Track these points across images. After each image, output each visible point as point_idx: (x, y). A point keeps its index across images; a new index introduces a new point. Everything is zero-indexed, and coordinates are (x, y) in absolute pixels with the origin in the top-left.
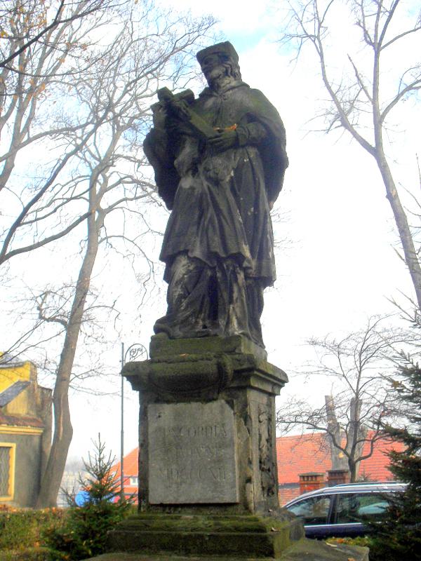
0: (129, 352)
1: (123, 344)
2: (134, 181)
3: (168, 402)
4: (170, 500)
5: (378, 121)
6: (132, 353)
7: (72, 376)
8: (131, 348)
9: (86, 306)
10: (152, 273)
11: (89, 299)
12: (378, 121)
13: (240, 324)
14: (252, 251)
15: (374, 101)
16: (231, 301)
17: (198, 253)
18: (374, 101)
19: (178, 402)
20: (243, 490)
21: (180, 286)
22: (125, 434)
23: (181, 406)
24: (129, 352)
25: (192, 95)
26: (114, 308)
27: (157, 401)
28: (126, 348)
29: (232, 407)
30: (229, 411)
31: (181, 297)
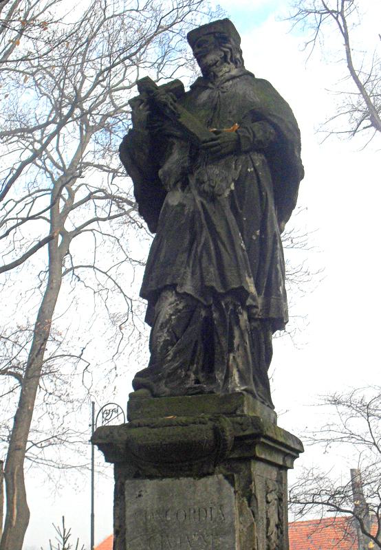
0: (101, 414)
3: (151, 477)
6: (105, 415)
7: (29, 445)
8: (104, 409)
11: (50, 347)
13: (242, 377)
14: (257, 286)
16: (231, 350)
19: (164, 477)
21: (166, 330)
24: (101, 414)
27: (137, 476)
28: (97, 409)
29: (232, 483)
30: (228, 489)
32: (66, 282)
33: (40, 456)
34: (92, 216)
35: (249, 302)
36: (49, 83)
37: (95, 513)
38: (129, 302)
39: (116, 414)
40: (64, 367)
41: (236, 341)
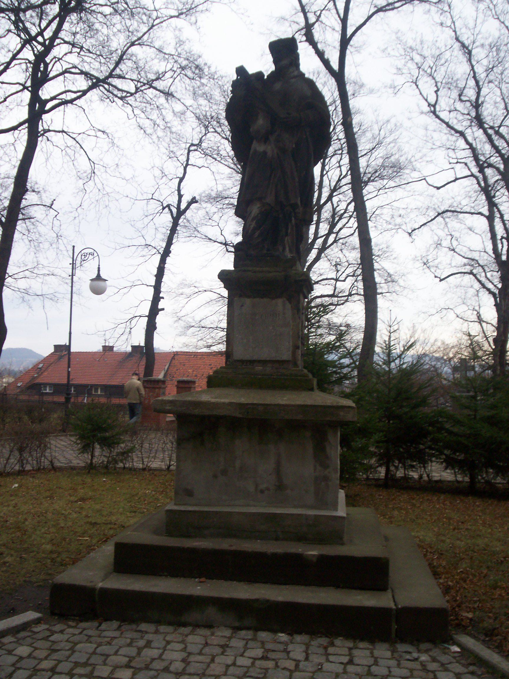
0: (80, 255)
1: (74, 247)
2: (82, 73)
3: (249, 297)
4: (248, 357)
5: (345, 42)
6: (83, 257)
7: (7, 276)
8: (83, 252)
9: (24, 203)
10: (93, 175)
11: (30, 198)
12: (345, 42)
13: (290, 250)
14: (301, 201)
15: (344, 21)
16: (287, 235)
17: (270, 199)
18: (344, 21)
19: (254, 297)
20: (294, 353)
21: (255, 222)
22: (72, 335)
23: (257, 300)
24: (80, 255)
25: (264, 76)
26: (53, 207)
27: (241, 296)
28: (77, 251)
29: (290, 303)
30: (288, 306)
31: (255, 229)
32: (42, 143)
33: (13, 285)
34: (63, 90)
35: (297, 211)
36: (398, 220)
37: (72, 331)
38: (93, 164)
39: (93, 257)
40: (37, 212)
41: (289, 230)
